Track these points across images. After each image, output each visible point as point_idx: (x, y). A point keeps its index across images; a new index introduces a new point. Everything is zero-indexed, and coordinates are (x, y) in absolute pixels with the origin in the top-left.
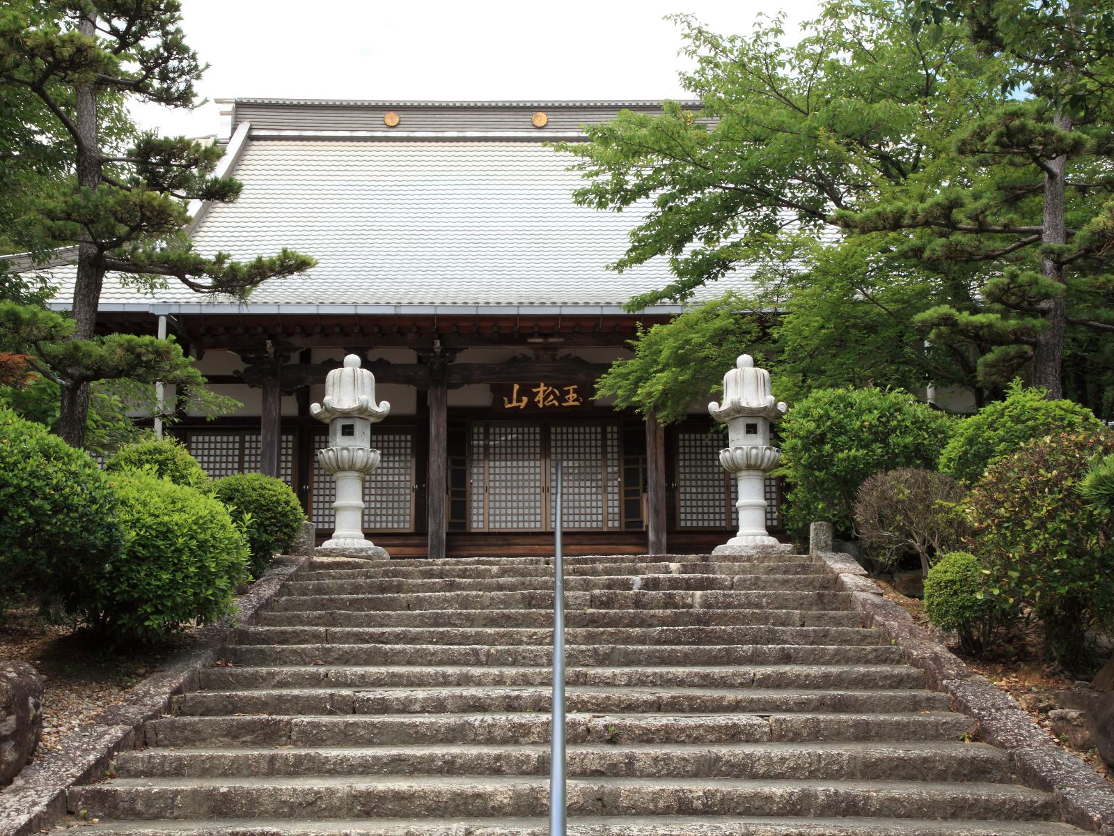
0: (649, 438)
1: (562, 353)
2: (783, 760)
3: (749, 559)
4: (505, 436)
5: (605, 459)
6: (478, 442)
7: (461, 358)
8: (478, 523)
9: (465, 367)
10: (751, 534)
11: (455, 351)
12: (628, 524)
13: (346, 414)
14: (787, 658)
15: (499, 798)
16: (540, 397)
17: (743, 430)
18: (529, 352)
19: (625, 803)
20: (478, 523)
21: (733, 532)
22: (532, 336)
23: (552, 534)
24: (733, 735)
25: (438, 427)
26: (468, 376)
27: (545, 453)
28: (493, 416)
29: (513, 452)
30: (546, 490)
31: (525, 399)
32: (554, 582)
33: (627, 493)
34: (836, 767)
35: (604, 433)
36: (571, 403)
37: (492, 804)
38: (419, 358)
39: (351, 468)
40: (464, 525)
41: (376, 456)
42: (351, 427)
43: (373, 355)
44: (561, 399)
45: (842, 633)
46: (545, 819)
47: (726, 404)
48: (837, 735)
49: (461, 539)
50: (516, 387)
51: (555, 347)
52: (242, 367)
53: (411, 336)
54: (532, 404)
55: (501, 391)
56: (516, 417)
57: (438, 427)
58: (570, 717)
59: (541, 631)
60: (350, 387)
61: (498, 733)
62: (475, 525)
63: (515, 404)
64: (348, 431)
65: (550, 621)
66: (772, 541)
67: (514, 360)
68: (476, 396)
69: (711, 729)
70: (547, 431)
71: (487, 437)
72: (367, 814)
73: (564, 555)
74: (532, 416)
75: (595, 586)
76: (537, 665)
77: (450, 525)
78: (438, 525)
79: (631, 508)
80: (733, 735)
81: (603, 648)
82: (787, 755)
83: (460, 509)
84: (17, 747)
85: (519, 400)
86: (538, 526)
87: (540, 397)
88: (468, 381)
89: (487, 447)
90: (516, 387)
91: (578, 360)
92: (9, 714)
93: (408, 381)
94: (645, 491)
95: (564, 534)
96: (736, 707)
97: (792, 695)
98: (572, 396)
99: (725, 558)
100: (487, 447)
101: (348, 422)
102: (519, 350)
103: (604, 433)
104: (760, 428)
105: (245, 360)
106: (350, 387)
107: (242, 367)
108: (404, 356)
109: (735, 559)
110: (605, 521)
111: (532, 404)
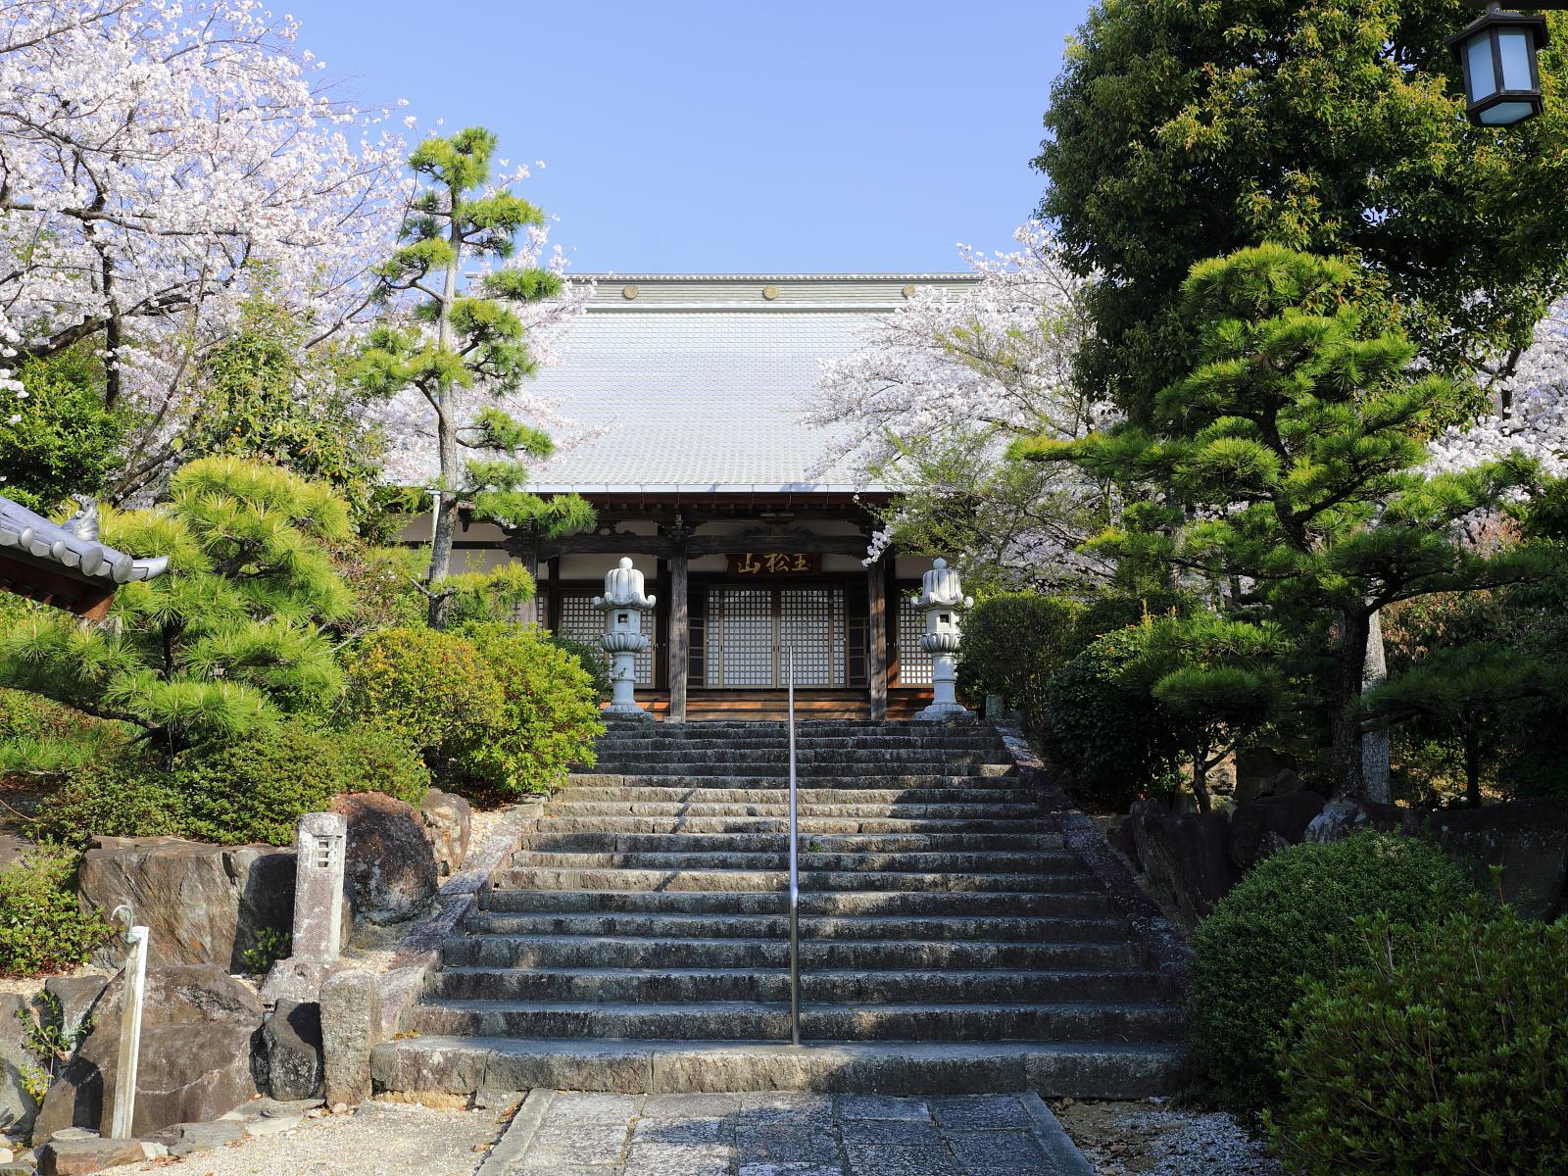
2: (934, 860)
5: (831, 615)
7: (700, 531)
8: (713, 680)
9: (706, 539)
11: (695, 524)
12: (852, 682)
16: (772, 562)
20: (713, 680)
22: (765, 511)
23: (787, 690)
26: (705, 548)
27: (776, 612)
28: (728, 580)
29: (745, 610)
30: (776, 649)
31: (758, 565)
33: (852, 652)
36: (800, 568)
38: (660, 531)
39: (626, 649)
40: (701, 682)
42: (625, 616)
44: (791, 565)
50: (749, 556)
54: (764, 569)
58: (802, 822)
61: (752, 846)
62: (710, 681)
63: (748, 569)
67: (749, 532)
68: (715, 563)
70: (777, 589)
71: (722, 596)
75: (818, 745)
83: (697, 667)
85: (752, 566)
86: (769, 683)
87: (772, 562)
90: (749, 556)
93: (652, 552)
95: (795, 690)
98: (801, 562)
100: (722, 608)
101: (623, 612)
109: (928, 724)
111: (764, 569)
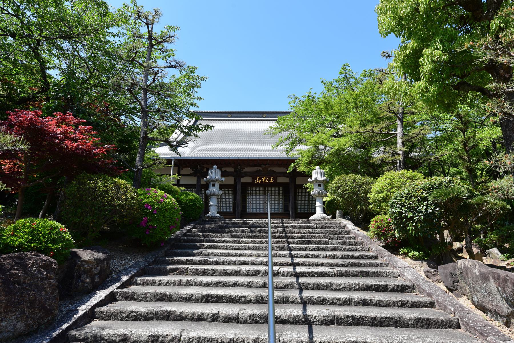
0: (290, 190)
1: (269, 169)
3: (320, 220)
4: (254, 189)
6: (249, 191)
7: (244, 170)
8: (248, 211)
9: (245, 172)
10: (319, 214)
11: (243, 169)
13: (213, 181)
14: (334, 249)
15: (250, 297)
16: (264, 180)
17: (317, 186)
18: (261, 169)
19: (291, 300)
20: (248, 211)
21: (315, 213)
23: (267, 213)
24: (322, 275)
25: (239, 187)
26: (246, 174)
28: (253, 184)
32: (268, 231)
33: (285, 204)
34: (357, 287)
35: (279, 189)
37: (248, 299)
39: (214, 195)
41: (221, 192)
43: (223, 169)
44: (269, 181)
45: (350, 242)
46: (265, 325)
47: (313, 179)
48: (355, 275)
49: (245, 214)
51: (267, 168)
52: (192, 172)
53: (232, 165)
54: (262, 182)
55: (254, 179)
56: (258, 185)
57: (239, 187)
59: (264, 240)
60: (214, 174)
64: (214, 185)
65: (267, 237)
66: (325, 215)
69: (316, 273)
72: (207, 301)
73: (271, 218)
74: (262, 184)
76: (262, 250)
77: (242, 211)
78: (239, 210)
79: (286, 207)
80: (322, 275)
81: (281, 245)
82: (341, 283)
84: (99, 277)
87: (264, 180)
88: (246, 176)
89: (251, 192)
91: (273, 171)
92: (98, 266)
93: (232, 176)
94: (289, 203)
95: (271, 213)
96: (322, 265)
97: (341, 261)
98: (272, 180)
99: (314, 220)
100: (251, 192)
102: (259, 168)
103: (279, 189)
104: (322, 186)
105: (193, 170)
106: (214, 174)
107: (192, 172)
108: (231, 170)
110: (279, 210)
111: (262, 182)
